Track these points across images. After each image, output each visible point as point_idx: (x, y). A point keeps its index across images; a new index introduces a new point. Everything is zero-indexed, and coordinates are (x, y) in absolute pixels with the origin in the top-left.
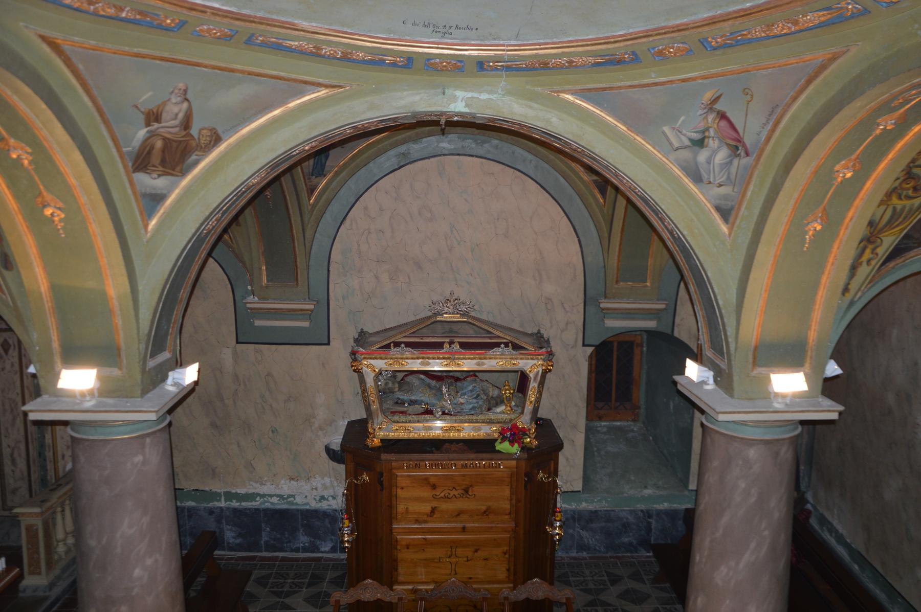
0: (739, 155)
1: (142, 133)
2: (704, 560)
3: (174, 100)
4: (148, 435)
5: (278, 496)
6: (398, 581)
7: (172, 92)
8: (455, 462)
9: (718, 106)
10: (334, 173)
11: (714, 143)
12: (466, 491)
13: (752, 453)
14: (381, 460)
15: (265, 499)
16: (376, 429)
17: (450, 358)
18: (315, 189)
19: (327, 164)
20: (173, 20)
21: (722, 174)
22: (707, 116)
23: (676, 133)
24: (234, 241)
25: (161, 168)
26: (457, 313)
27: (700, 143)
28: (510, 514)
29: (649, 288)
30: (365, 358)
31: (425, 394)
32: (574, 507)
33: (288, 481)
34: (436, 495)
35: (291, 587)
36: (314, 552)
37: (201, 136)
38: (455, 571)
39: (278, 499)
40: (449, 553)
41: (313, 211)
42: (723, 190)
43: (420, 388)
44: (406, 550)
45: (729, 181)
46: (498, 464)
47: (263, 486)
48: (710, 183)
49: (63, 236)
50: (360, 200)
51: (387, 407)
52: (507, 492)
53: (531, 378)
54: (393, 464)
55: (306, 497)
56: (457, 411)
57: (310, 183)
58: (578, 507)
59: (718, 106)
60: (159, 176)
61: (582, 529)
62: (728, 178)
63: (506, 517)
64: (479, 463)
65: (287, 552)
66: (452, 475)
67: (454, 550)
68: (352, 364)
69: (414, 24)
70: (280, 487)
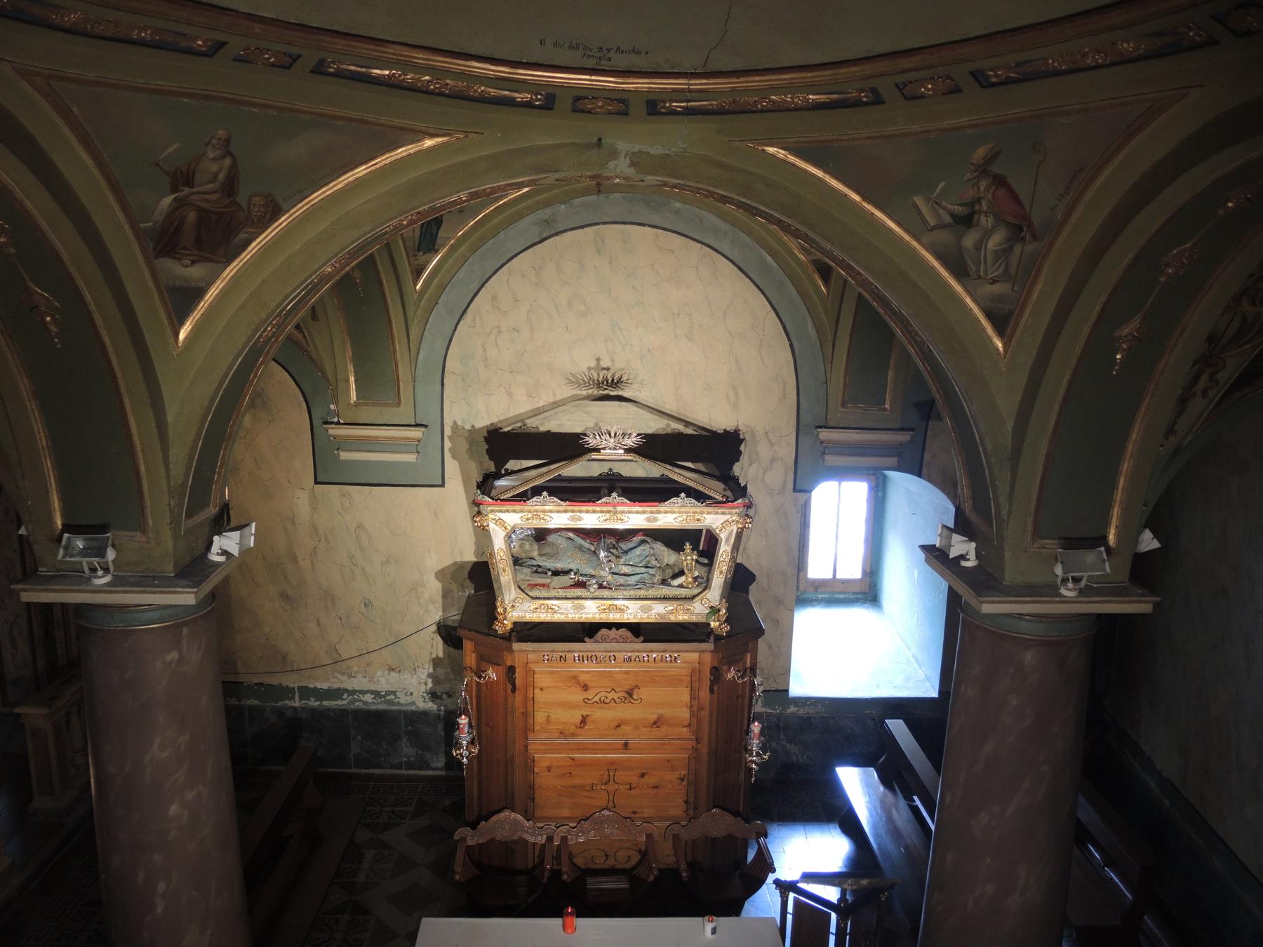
0: (1023, 239)
1: (167, 201)
3: (211, 155)
4: (185, 624)
7: (209, 143)
10: (449, 248)
11: (987, 221)
13: (1028, 657)
14: (513, 651)
15: (356, 697)
18: (424, 269)
19: (440, 234)
20: (204, 42)
21: (996, 265)
24: (310, 342)
26: (620, 448)
27: (965, 221)
28: (689, 726)
29: (888, 412)
30: (492, 511)
31: (574, 560)
32: (778, 711)
33: (386, 672)
36: (420, 768)
39: (373, 696)
40: (606, 778)
41: (421, 301)
42: (997, 288)
46: (673, 658)
48: (979, 277)
49: (59, 346)
50: (486, 286)
51: (523, 577)
52: (685, 696)
53: (721, 540)
54: (529, 656)
55: (411, 694)
56: (618, 584)
57: (416, 262)
59: (996, 168)
60: (193, 262)
61: (789, 742)
62: (1006, 271)
63: (685, 729)
65: (386, 768)
66: (609, 672)
67: (611, 774)
68: (475, 519)
69: (556, 45)
70: (375, 680)
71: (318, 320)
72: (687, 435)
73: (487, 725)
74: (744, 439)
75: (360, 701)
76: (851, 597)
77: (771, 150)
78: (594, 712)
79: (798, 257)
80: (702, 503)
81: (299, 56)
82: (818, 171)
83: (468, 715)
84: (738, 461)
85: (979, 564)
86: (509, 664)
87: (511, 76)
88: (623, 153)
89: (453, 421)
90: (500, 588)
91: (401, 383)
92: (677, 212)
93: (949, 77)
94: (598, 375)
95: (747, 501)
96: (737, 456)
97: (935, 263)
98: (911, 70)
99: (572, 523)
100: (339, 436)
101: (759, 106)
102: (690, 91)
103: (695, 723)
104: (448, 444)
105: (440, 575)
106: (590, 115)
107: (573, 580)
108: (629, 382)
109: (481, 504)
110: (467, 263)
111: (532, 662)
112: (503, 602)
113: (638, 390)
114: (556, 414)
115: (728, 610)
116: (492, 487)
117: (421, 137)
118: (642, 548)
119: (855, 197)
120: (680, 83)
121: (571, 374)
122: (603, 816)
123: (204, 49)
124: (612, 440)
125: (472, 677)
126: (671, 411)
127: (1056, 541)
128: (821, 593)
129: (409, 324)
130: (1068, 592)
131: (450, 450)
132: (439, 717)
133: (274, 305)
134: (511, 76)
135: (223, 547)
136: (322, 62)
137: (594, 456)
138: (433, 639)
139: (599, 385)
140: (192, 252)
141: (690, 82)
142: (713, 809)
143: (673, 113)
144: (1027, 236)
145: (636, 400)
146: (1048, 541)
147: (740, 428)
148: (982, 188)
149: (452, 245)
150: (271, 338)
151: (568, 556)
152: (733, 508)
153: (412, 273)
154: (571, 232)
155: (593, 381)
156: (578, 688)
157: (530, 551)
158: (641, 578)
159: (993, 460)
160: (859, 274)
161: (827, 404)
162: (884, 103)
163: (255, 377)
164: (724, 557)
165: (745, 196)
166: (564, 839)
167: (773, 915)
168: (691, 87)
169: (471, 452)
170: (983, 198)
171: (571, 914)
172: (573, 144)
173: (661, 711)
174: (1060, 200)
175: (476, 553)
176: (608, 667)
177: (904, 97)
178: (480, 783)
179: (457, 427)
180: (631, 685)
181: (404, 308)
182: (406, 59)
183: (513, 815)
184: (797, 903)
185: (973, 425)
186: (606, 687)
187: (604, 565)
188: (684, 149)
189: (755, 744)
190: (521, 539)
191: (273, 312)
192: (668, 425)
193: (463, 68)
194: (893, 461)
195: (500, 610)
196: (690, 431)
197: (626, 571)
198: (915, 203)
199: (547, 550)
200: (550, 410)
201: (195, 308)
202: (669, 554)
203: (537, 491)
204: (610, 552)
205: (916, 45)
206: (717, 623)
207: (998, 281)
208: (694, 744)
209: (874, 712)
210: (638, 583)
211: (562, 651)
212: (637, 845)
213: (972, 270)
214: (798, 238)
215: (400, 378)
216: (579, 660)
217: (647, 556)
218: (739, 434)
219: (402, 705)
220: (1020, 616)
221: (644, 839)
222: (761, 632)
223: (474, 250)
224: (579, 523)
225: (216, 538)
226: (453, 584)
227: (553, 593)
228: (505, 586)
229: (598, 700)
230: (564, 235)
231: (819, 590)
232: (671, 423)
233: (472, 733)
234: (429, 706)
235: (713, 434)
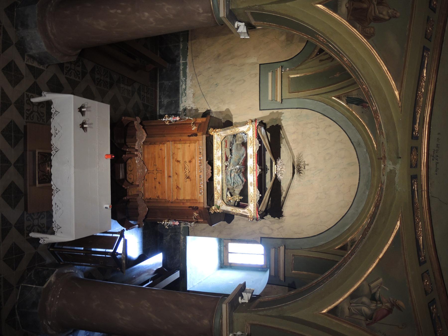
0: (367, 320)
4: (212, 15)
5: (186, 88)
6: (145, 145)
7: (394, 10)
8: (202, 172)
9: (395, 309)
11: (373, 306)
12: (188, 178)
13: (206, 322)
14: (203, 135)
15: (184, 82)
16: (218, 133)
17: (254, 169)
20: (435, 5)
23: (379, 285)
24: (311, 60)
27: (373, 298)
28: (177, 199)
30: (253, 126)
31: (236, 157)
32: (181, 232)
33: (193, 93)
34: (186, 163)
35: (142, 95)
36: (159, 106)
38: (150, 173)
39: (184, 88)
40: (158, 170)
41: (328, 99)
42: (347, 311)
43: (238, 154)
46: (201, 193)
47: (190, 81)
48: (351, 304)
52: (188, 198)
53: (244, 210)
55: (185, 102)
56: (227, 173)
57: (343, 96)
58: (181, 234)
59: (395, 309)
60: (347, 8)
61: (171, 236)
62: (354, 314)
63: (176, 198)
64: (202, 184)
66: (196, 170)
67: (160, 172)
68: (250, 120)
69: (438, 139)
70: (190, 89)
71: (319, 62)
72: (281, 198)
73: (176, 127)
74: (280, 219)
75: (183, 84)
76: (222, 259)
77: (399, 223)
78: (182, 165)
80: (257, 202)
81: (430, 41)
82: (391, 242)
83: (180, 119)
84: (272, 217)
85: (240, 304)
86: (198, 134)
87: (425, 122)
90: (225, 130)
92: (364, 193)
93: (432, 290)
95: (259, 219)
96: (273, 216)
97: (355, 287)
98: (434, 276)
99: (249, 155)
100: (277, 72)
102: (422, 191)
103: (178, 201)
104: (275, 111)
105: (228, 110)
108: (300, 176)
109: (256, 122)
110: (342, 115)
111: (199, 142)
112: (220, 131)
113: (297, 179)
114: (288, 150)
115: (219, 212)
116: (261, 126)
117: (399, 90)
118: (240, 181)
119: (381, 256)
120: (425, 187)
121: (302, 155)
122: (145, 169)
123: (432, 5)
124: (280, 169)
125: (193, 121)
126: (290, 192)
127: (249, 333)
128: (223, 248)
129: (320, 95)
131: (273, 112)
132: (178, 112)
133: (332, 39)
134: (425, 122)
135: (240, 26)
136: (428, 50)
137: (274, 163)
138: (205, 109)
139: (298, 165)
140: (351, 6)
141: (425, 191)
142: (148, 208)
143: (412, 185)
146: (249, 329)
147: (284, 217)
148: (387, 304)
149: (350, 109)
150: (318, 40)
152: (256, 213)
153: (339, 95)
154: (356, 154)
155: (300, 163)
156: (190, 159)
157: (238, 140)
158: (229, 181)
159: (280, 309)
160: (350, 258)
161: (294, 249)
162: (420, 266)
163: (303, 35)
164: (238, 211)
165: (379, 214)
166: (137, 155)
167: (112, 228)
168: (423, 192)
169: (272, 120)
172: (398, 148)
173: (182, 189)
176: (197, 170)
177: (423, 274)
178: (156, 125)
179: (282, 114)
180: (191, 178)
181: (325, 93)
182: (431, 82)
183: (145, 138)
184: (116, 238)
185: (293, 301)
186: (190, 169)
187: (234, 167)
188: (398, 190)
189: (171, 223)
190: (243, 137)
191: (329, 39)
192: (284, 191)
193: (428, 104)
194: (273, 274)
195: (217, 130)
196: (282, 199)
198: (380, 279)
199: (239, 147)
201: (330, 10)
202: (238, 191)
203: (260, 142)
204: (239, 169)
206: (214, 209)
207: (349, 311)
208: (171, 201)
209: (182, 267)
210: (228, 180)
211: (203, 152)
212: (135, 181)
214: (362, 235)
216: (200, 159)
217: (237, 183)
218: (281, 217)
220: (221, 318)
221: (137, 184)
222: (211, 225)
223: (348, 118)
224: (250, 157)
225: (244, 24)
226: (225, 115)
227: (223, 149)
228: (226, 132)
229: (185, 166)
230: (355, 151)
231: (224, 247)
232: (285, 192)
233: (173, 122)
235: (281, 208)
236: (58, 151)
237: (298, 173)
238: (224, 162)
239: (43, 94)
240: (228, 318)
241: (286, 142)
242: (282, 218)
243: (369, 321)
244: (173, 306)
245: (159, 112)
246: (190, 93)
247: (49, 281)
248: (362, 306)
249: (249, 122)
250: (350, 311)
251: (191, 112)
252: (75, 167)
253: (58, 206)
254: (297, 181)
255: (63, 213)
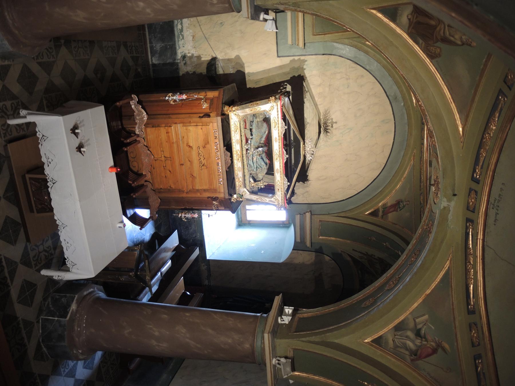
0: (411, 356)
2: (187, 319)
3: (463, 37)
11: (418, 342)
17: (280, 155)
21: (400, 343)
22: (434, 342)
25: (415, 21)
27: (418, 334)
33: (192, 34)
36: (151, 53)
37: (435, 48)
39: (180, 29)
41: (361, 43)
42: (391, 342)
43: (260, 133)
44: (165, 132)
45: (396, 347)
48: (395, 335)
54: (215, 123)
55: (184, 47)
56: (249, 157)
59: (440, 350)
60: (409, 19)
62: (398, 347)
63: (191, 187)
67: (169, 159)
69: (502, 189)
70: (188, 29)
74: (305, 183)
76: (240, 217)
79: (380, 202)
88: (449, 204)
89: (307, 60)
90: (243, 108)
91: (323, 36)
94: (330, 123)
101: (468, 264)
104: (296, 58)
105: (238, 57)
106: (468, 195)
107: (249, 138)
108: (327, 136)
112: (237, 110)
118: (264, 165)
119: (428, 292)
130: (274, 361)
131: (294, 59)
132: (175, 60)
138: (209, 55)
139: (325, 123)
141: (481, 240)
144: (412, 357)
145: (319, 138)
147: (309, 182)
148: (432, 343)
151: (258, 134)
155: (327, 121)
169: (293, 69)
170: (428, 343)
171: (117, 171)
172: (454, 185)
173: (198, 177)
174: (428, 373)
175: (249, 73)
179: (305, 62)
195: (234, 109)
197: (254, 159)
198: (425, 315)
200: (314, 103)
205: (492, 333)
209: (198, 236)
212: (141, 169)
213: (398, 333)
215: (326, 35)
219: (178, 42)
226: (235, 63)
228: (244, 111)
230: (390, 106)
234: (179, 55)
236: (55, 183)
237: (324, 132)
238: (244, 145)
239: (21, 112)
240: (271, 346)
241: (311, 96)
242: (307, 182)
243: (414, 357)
244: (210, 331)
245: (152, 60)
246: (188, 35)
247: (71, 311)
248: (407, 340)
249: (272, 99)
250: (395, 342)
251: (192, 60)
252: (80, 201)
253: (68, 242)
254: (324, 141)
255: (75, 250)
